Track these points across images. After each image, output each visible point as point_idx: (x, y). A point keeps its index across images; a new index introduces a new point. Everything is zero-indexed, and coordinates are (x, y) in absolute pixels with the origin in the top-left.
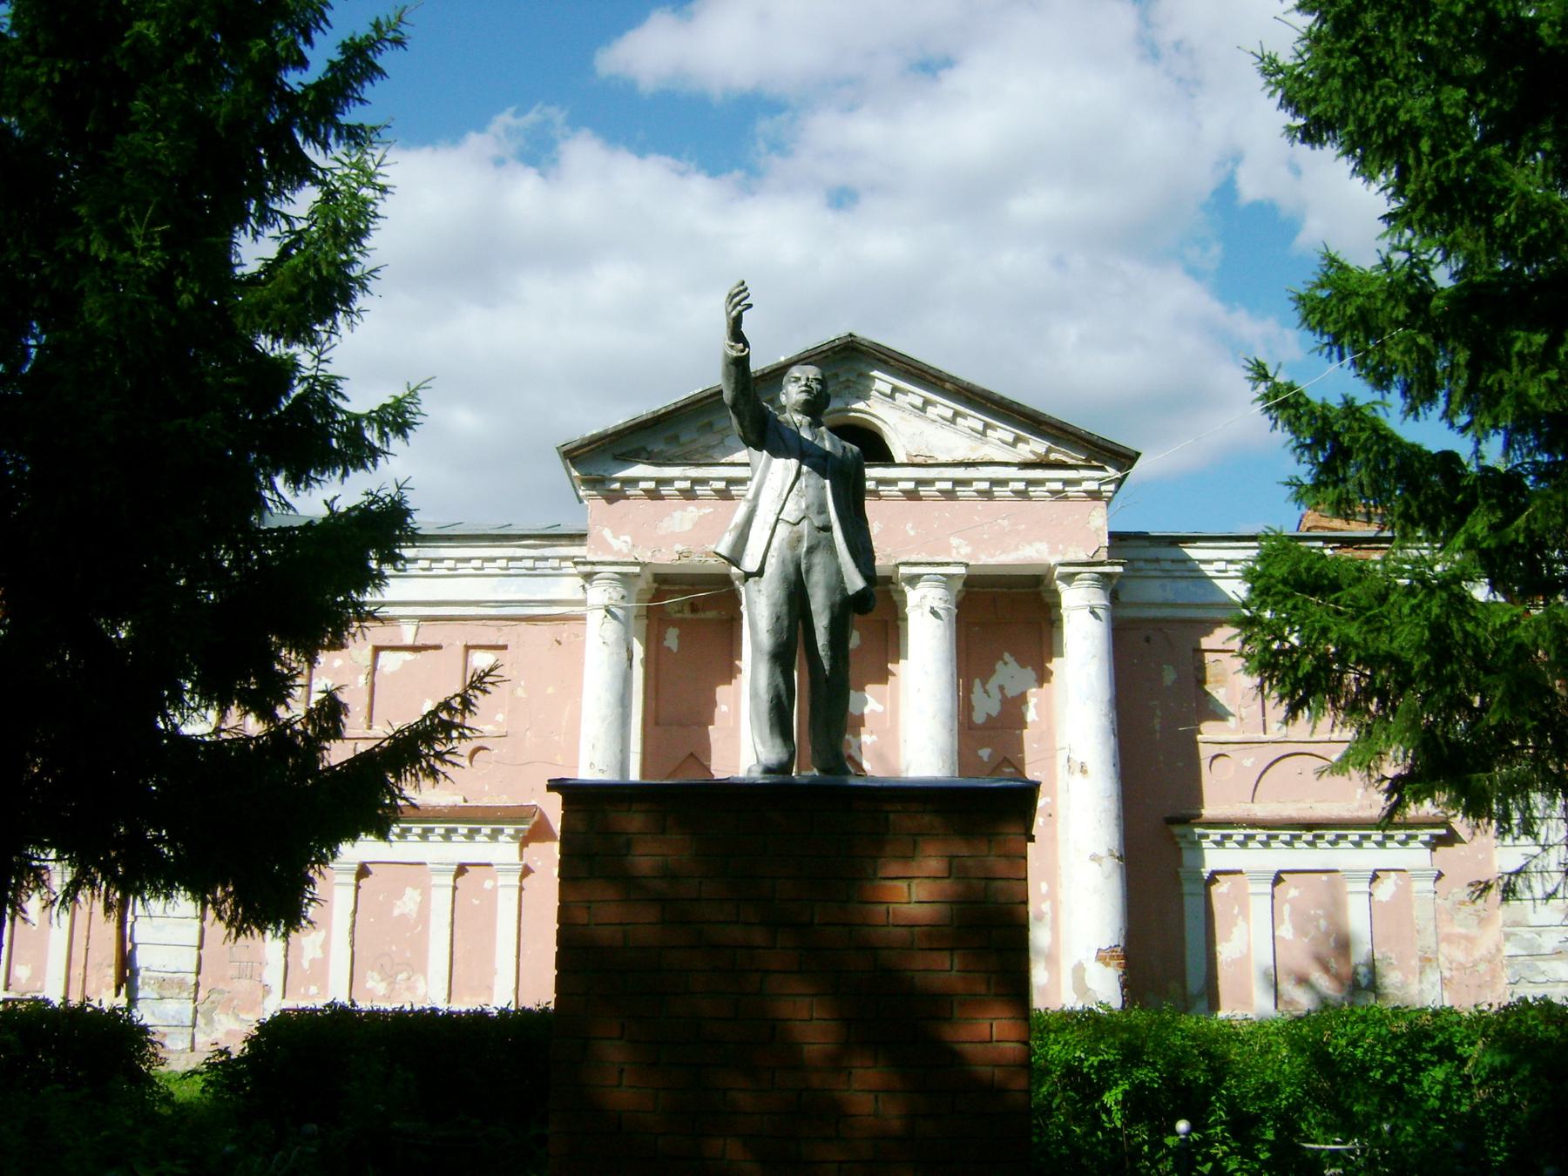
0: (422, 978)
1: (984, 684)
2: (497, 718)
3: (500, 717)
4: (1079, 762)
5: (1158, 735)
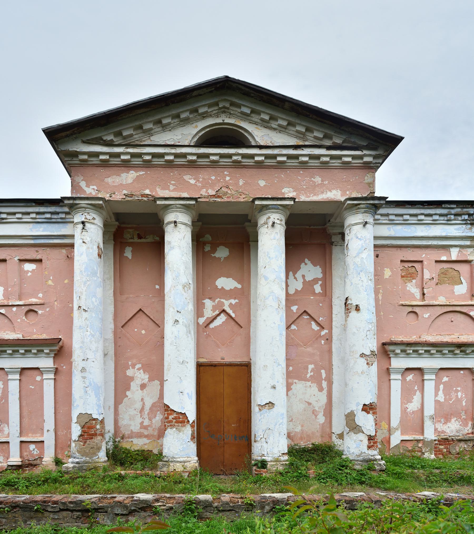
0: (6, 425)
1: (294, 275)
2: (39, 296)
3: (40, 295)
4: (355, 304)
5: (380, 302)
